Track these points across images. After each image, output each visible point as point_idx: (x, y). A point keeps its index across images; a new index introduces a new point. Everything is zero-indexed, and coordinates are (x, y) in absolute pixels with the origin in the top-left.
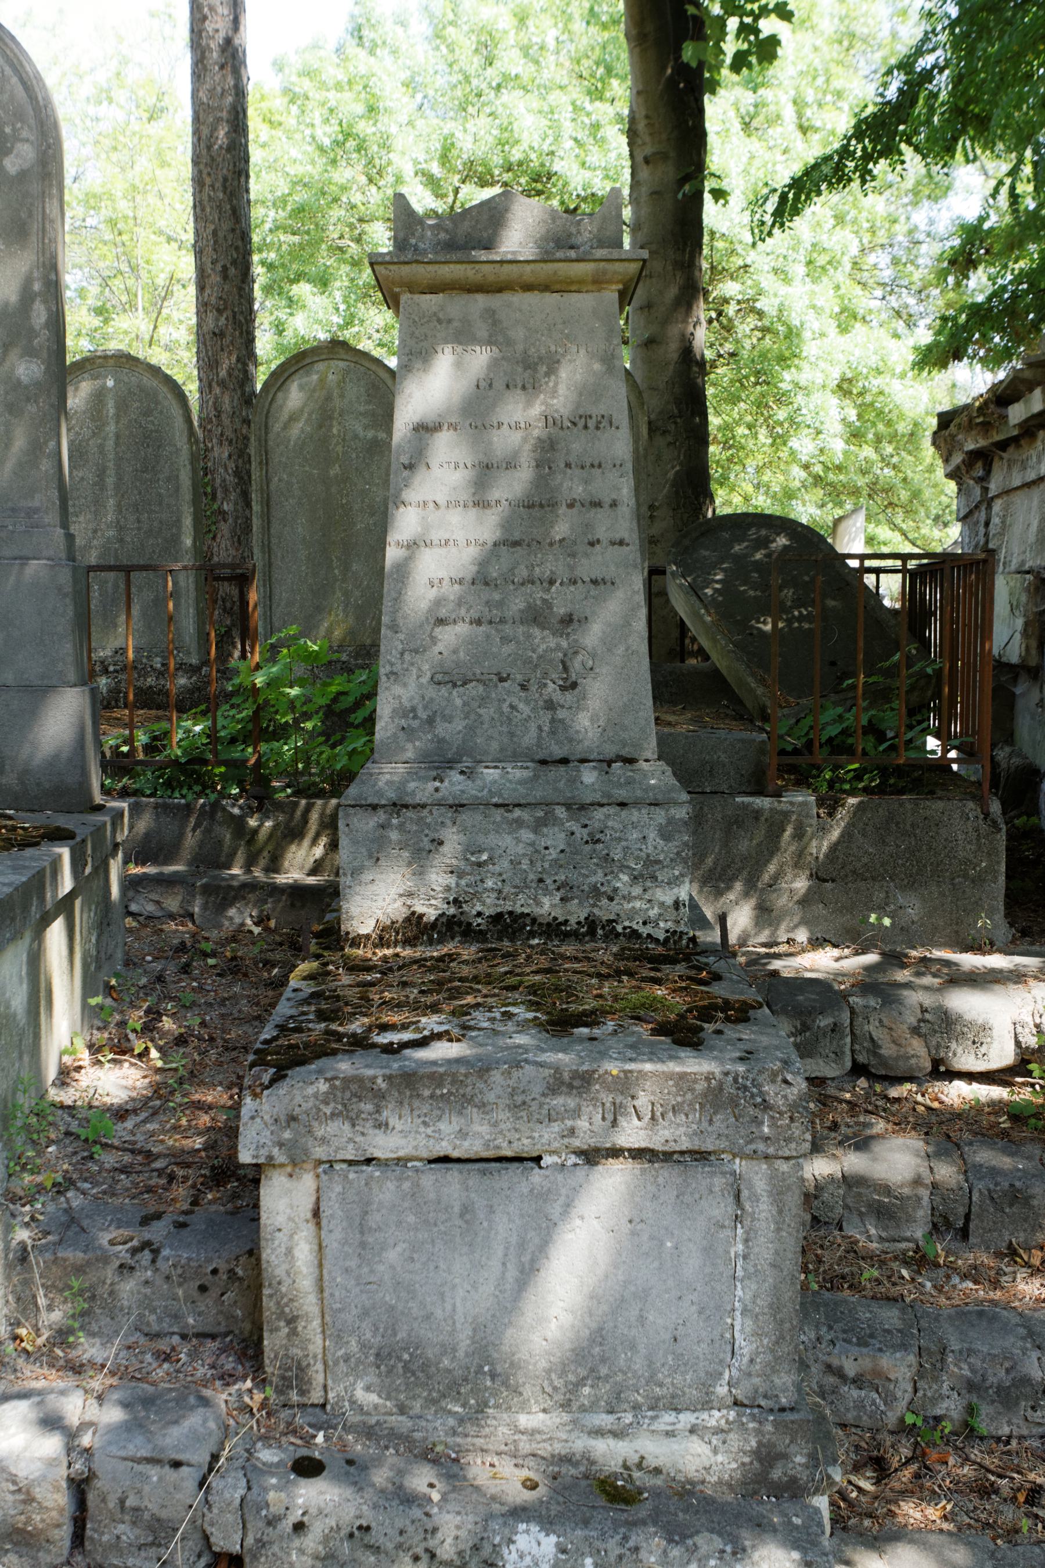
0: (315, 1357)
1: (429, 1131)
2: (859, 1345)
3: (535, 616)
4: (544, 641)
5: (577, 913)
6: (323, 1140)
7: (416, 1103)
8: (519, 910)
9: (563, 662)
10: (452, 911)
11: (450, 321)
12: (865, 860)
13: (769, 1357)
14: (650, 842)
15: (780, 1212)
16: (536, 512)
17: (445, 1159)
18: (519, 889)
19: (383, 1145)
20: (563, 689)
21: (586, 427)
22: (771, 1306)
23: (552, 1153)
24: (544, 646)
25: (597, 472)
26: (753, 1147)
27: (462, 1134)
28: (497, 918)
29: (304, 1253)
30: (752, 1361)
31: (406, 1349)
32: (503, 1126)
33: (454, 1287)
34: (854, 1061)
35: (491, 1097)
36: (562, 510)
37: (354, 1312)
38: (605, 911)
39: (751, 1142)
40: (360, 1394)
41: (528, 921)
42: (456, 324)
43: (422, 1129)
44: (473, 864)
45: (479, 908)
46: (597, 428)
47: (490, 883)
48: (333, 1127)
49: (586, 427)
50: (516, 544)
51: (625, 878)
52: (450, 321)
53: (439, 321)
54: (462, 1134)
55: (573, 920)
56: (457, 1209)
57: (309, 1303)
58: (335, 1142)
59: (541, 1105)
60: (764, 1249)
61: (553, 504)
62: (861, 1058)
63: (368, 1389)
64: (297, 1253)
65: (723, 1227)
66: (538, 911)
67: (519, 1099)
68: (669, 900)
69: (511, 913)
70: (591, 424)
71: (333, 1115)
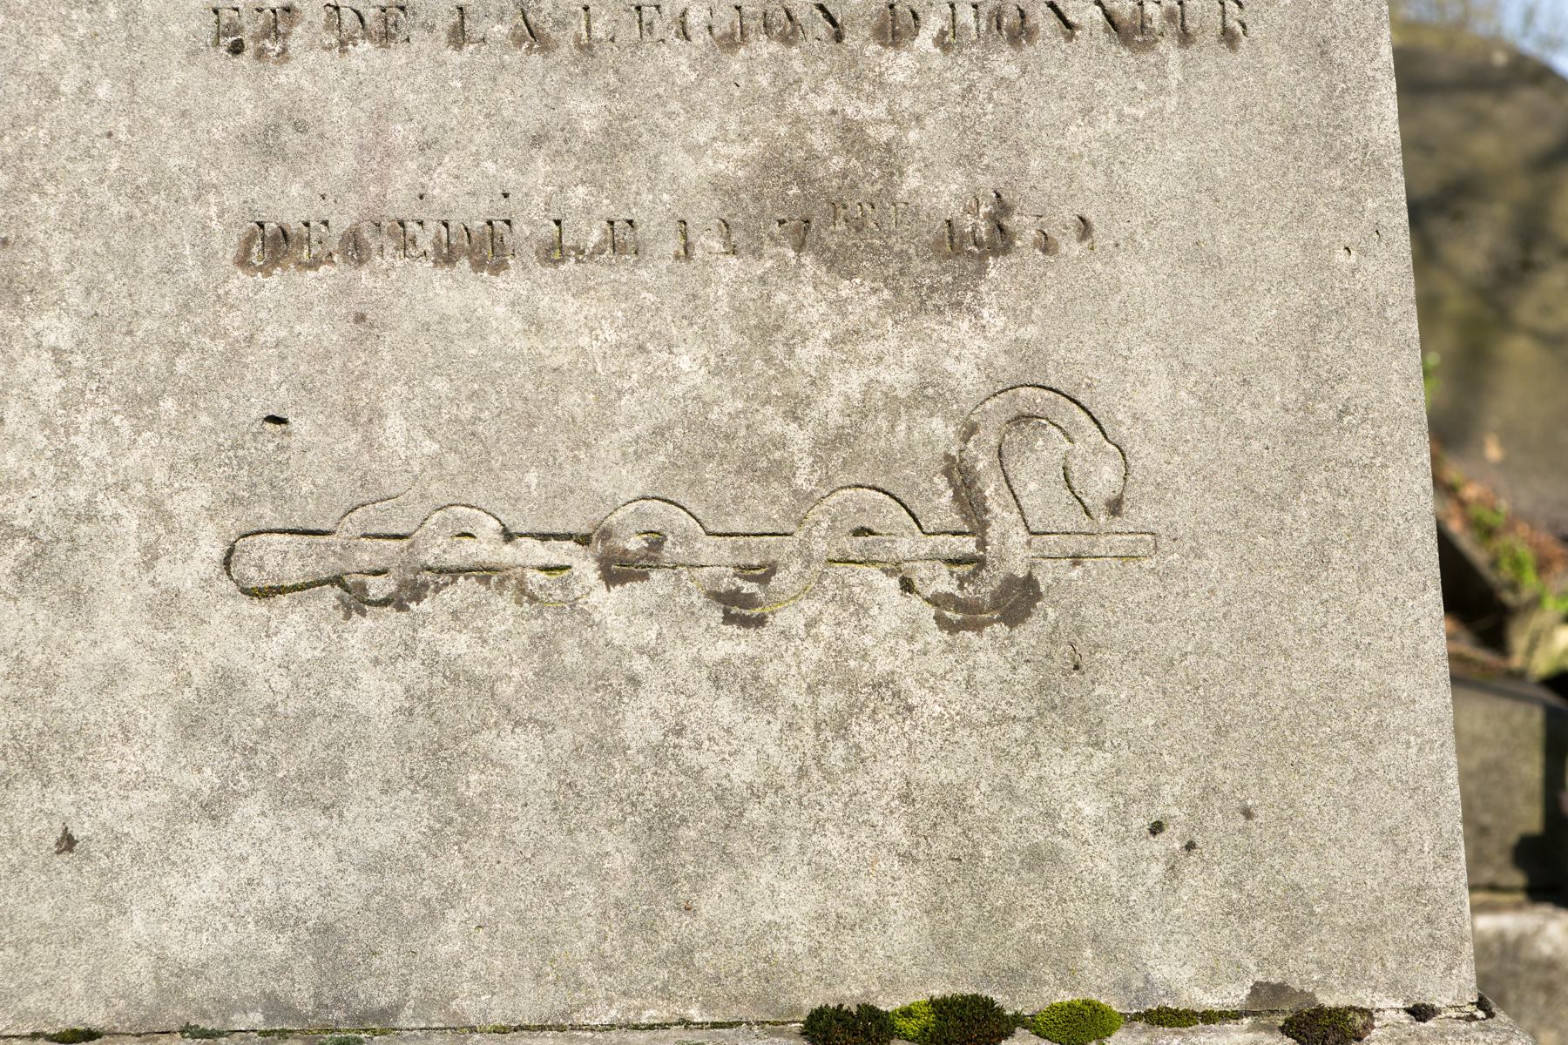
3: (814, 214)
4: (867, 355)
20: (958, 616)
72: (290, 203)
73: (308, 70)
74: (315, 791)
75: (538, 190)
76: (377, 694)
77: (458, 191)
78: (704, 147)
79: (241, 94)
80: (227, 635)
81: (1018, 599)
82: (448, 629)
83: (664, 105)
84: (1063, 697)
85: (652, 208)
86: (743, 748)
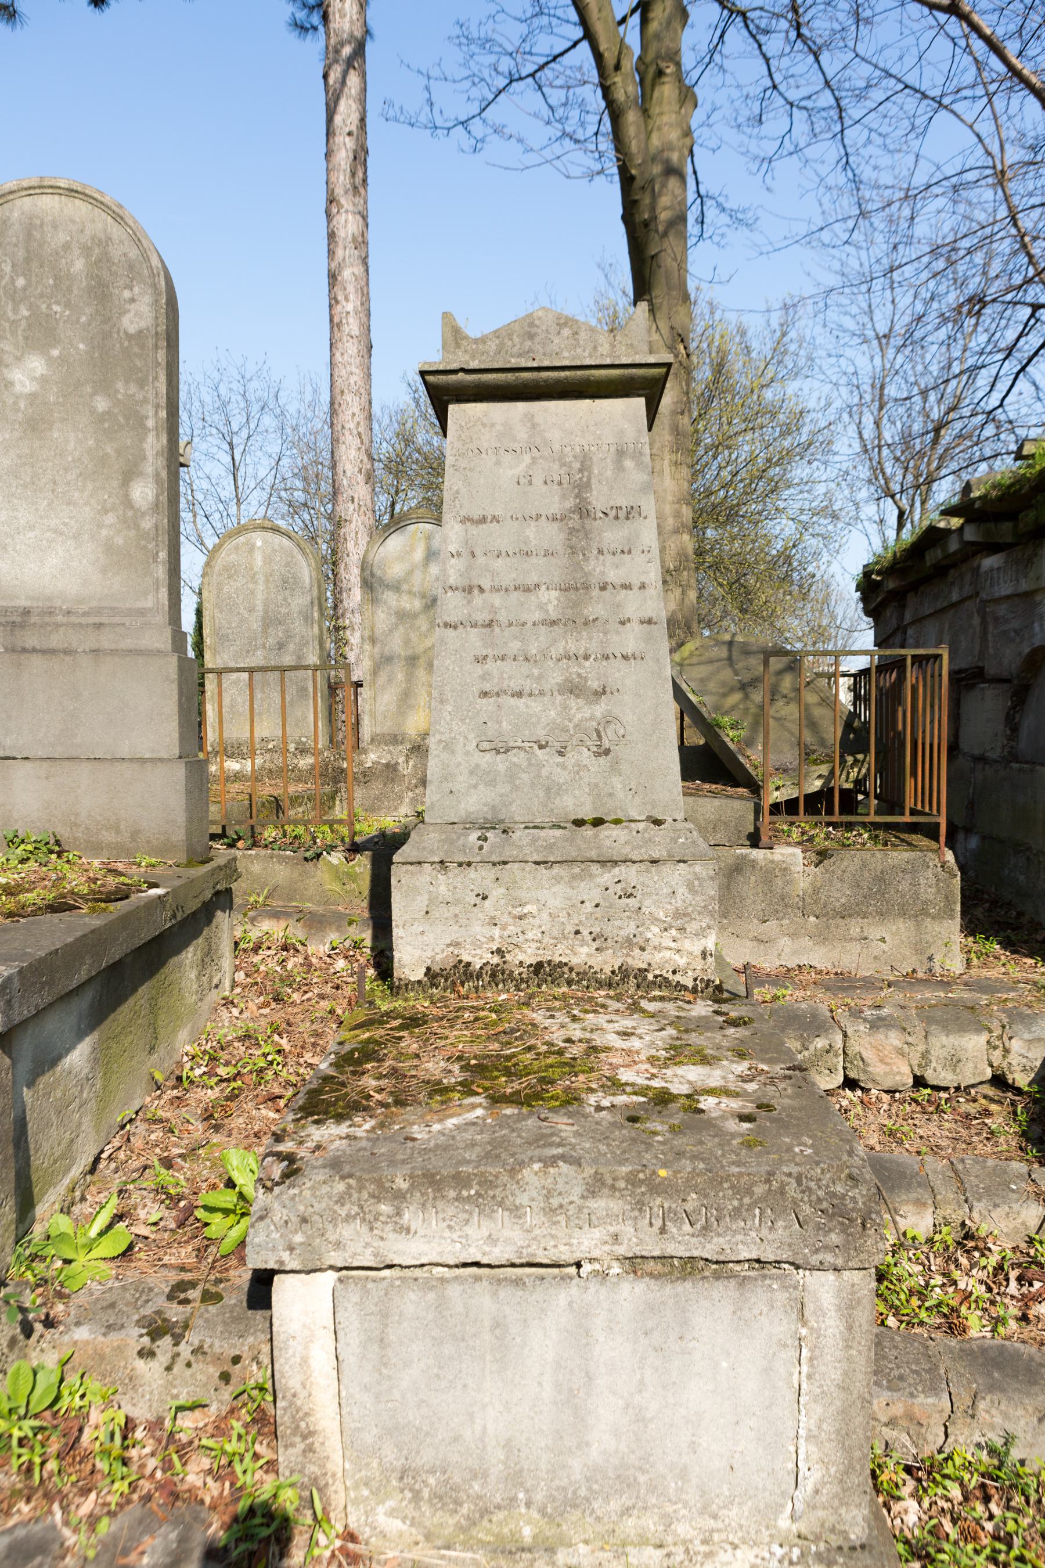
0: (334, 1475)
1: (455, 1236)
2: (890, 1389)
3: (573, 689)
4: (581, 711)
5: (606, 962)
6: (338, 1245)
7: (440, 1204)
8: (557, 959)
9: (598, 732)
10: (496, 960)
11: (493, 425)
12: (843, 900)
13: (836, 1488)
14: (679, 895)
15: (850, 1328)
16: (572, 594)
18: (557, 941)
19: (406, 1250)
20: (598, 755)
21: (617, 518)
22: (838, 1432)
23: (591, 1260)
24: (579, 716)
25: (626, 557)
26: (820, 1256)
27: (491, 1239)
28: (539, 966)
29: (321, 1360)
30: (817, 1492)
31: (432, 1471)
32: (537, 1232)
33: (484, 1407)
34: (846, 1076)
35: (522, 1199)
36: (595, 593)
37: (375, 1431)
38: (638, 960)
39: (817, 1251)
40: (382, 1519)
41: (566, 969)
42: (498, 427)
43: (447, 1233)
44: (515, 917)
45: (521, 957)
46: (628, 518)
47: (530, 935)
48: (346, 1231)
49: (617, 518)
50: (553, 623)
51: (656, 930)
52: (493, 425)
53: (484, 425)
54: (491, 1239)
55: (607, 970)
56: (487, 1323)
57: (325, 1417)
58: (352, 1247)
59: (580, 1209)
60: (832, 1372)
61: (587, 588)
62: (852, 1075)
63: (391, 1513)
64: (314, 1364)
65: (785, 1346)
66: (575, 961)
67: (555, 1202)
68: (697, 950)
69: (549, 962)
70: (622, 514)
71: (349, 1218)
72: (487, 687)
73: (490, 666)
74: (492, 783)
75: (528, 685)
76: (502, 768)
77: (514, 685)
78: (555, 678)
79: (479, 670)
81: (607, 752)
82: (514, 757)
85: (547, 687)
86: (561, 777)
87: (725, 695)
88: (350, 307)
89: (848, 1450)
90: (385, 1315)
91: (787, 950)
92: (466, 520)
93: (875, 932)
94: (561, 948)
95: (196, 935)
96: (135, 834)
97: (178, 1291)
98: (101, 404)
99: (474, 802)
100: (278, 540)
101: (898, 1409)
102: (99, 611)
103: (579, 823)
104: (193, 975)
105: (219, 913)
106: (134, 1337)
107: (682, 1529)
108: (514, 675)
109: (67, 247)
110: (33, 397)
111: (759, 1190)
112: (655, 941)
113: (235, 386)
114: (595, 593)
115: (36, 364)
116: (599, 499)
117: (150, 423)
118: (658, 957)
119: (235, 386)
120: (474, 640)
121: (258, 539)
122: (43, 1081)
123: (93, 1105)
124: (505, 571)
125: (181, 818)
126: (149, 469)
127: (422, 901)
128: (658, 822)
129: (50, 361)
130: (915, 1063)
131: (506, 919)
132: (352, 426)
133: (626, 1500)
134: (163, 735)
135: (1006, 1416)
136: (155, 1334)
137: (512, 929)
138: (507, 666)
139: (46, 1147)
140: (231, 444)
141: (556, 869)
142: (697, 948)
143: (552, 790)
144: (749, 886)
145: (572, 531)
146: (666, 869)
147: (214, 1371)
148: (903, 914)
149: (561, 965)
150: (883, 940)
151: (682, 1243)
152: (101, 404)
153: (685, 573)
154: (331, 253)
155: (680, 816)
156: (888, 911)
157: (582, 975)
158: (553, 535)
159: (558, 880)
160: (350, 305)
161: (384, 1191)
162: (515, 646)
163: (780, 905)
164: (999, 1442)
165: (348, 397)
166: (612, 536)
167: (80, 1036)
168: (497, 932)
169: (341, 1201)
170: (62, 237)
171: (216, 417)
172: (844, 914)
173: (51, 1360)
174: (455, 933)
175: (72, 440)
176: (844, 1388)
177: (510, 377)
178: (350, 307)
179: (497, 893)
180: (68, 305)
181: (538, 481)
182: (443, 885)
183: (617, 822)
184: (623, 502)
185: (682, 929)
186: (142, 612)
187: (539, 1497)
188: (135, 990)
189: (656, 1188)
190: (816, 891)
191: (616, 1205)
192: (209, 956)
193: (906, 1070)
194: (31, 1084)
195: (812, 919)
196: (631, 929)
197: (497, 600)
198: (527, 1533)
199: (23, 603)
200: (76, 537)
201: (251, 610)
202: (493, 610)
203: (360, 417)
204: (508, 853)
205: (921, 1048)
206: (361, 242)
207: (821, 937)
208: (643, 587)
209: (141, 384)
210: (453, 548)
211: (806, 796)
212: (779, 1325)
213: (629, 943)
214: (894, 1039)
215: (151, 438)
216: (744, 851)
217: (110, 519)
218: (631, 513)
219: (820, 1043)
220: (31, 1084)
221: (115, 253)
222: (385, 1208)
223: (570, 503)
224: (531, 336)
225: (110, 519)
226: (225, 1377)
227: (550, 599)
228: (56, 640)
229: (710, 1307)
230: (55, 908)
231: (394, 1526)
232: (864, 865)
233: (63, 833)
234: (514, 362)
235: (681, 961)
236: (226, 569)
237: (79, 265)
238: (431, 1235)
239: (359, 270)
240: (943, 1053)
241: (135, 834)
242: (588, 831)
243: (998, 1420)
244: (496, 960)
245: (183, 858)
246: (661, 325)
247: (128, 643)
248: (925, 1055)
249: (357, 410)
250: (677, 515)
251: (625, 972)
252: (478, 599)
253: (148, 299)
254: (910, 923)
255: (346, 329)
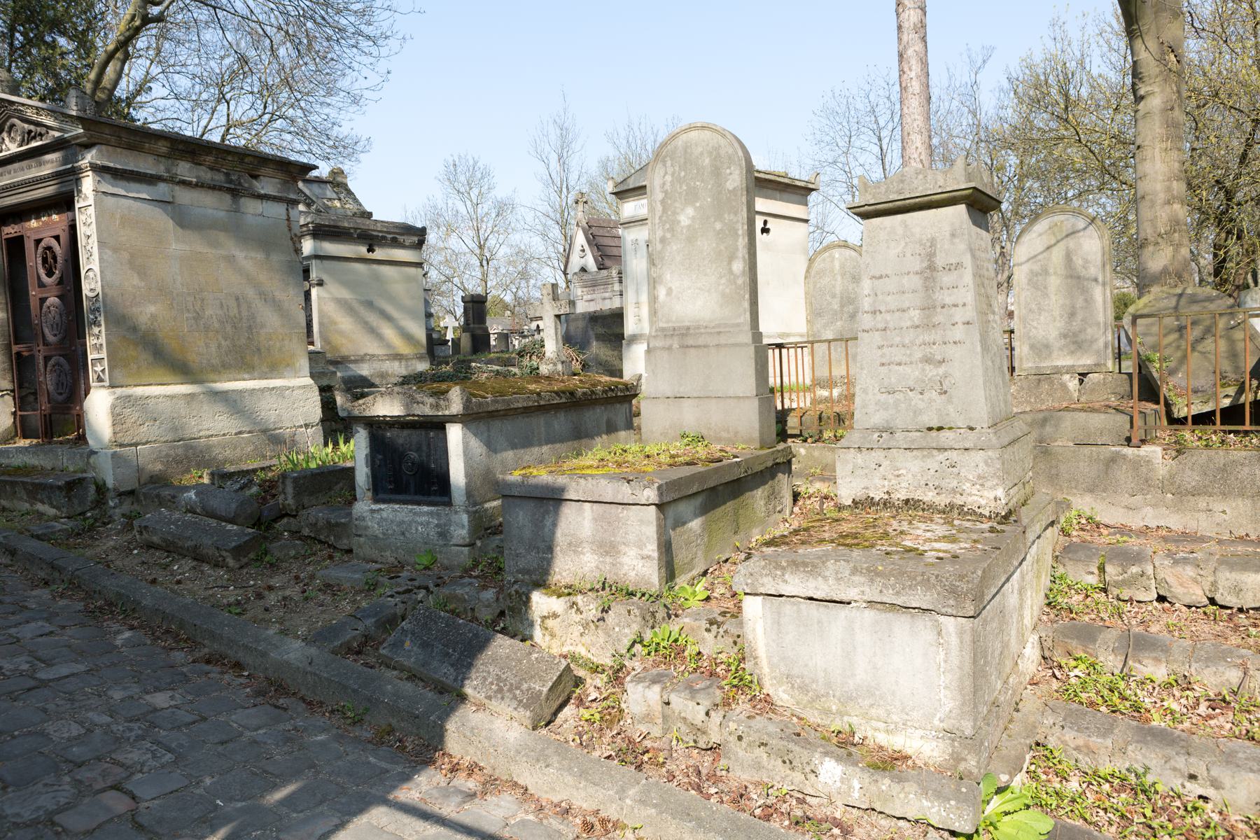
3: (928, 360)
4: (932, 372)
5: (942, 501)
6: (763, 585)
10: (886, 497)
16: (927, 312)
17: (811, 599)
18: (916, 488)
20: (940, 394)
28: (907, 501)
35: (827, 574)
36: (939, 310)
38: (959, 501)
48: (765, 580)
57: (762, 652)
60: (955, 661)
63: (784, 691)
66: (925, 499)
72: (884, 361)
73: (885, 350)
74: (886, 409)
75: (904, 359)
76: (891, 401)
77: (897, 359)
78: (918, 355)
79: (880, 352)
80: (879, 396)
81: (945, 392)
82: (897, 396)
83: (134, 814)
84: (950, 401)
85: (914, 360)
86: (921, 405)
87: (1165, 335)
88: (913, 74)
89: (964, 696)
90: (779, 613)
91: (1149, 515)
92: (873, 277)
93: (1218, 506)
94: (918, 492)
95: (764, 483)
96: (736, 433)
97: (723, 614)
98: (718, 226)
99: (878, 419)
100: (848, 252)
101: (1080, 742)
102: (719, 326)
103: (930, 429)
104: (762, 503)
105: (780, 475)
106: (705, 624)
107: (895, 718)
108: (898, 355)
109: (702, 154)
110: (689, 226)
111: (919, 578)
112: (968, 491)
113: (881, 92)
114: (939, 310)
115: (690, 211)
116: (940, 261)
117: (740, 232)
118: (970, 499)
119: (881, 92)
120: (877, 337)
121: (837, 253)
122: (678, 530)
123: (702, 547)
124: (893, 303)
125: (757, 426)
126: (740, 255)
127: (850, 467)
128: (972, 429)
129: (696, 209)
130: (1207, 588)
131: (890, 476)
132: (916, 156)
133: (871, 701)
134: (748, 385)
135: (1144, 756)
136: (711, 623)
137: (893, 482)
138: (893, 350)
139: (680, 557)
140: (880, 140)
141: (915, 452)
142: (991, 495)
143: (917, 412)
144: (1122, 474)
145: (926, 279)
146: (972, 453)
147: (731, 640)
148: (1242, 495)
149: (919, 501)
150: (1224, 512)
151: (888, 598)
152: (718, 226)
153: (1176, 235)
154: (900, 39)
155: (985, 426)
156: (1230, 493)
157: (930, 507)
158: (916, 282)
159: (916, 458)
160: (914, 70)
161: (778, 566)
162: (898, 339)
163: (1145, 482)
164: (1141, 771)
165: (913, 137)
166: (946, 279)
167: (696, 516)
168: (886, 483)
169: (763, 568)
170: (700, 149)
171: (868, 119)
172: (1195, 492)
173: (676, 629)
174: (866, 482)
175: (706, 245)
176: (960, 668)
177: (890, 205)
178: (913, 74)
179: (885, 463)
180: (702, 181)
181: (908, 255)
182: (860, 459)
183: (950, 428)
184: (954, 261)
185: (982, 485)
186: (738, 325)
187: (838, 694)
188: (724, 503)
189: (878, 574)
190: (1172, 476)
191: (863, 579)
192: (773, 496)
193: (1200, 592)
194: (674, 529)
195: (1169, 495)
196: (955, 484)
197: (888, 317)
198: (834, 708)
199: (687, 324)
200: (709, 291)
201: (834, 296)
202: (887, 322)
203: (922, 149)
204: (892, 444)
205: (1211, 579)
206: (921, 28)
207: (1177, 507)
208: (964, 305)
209: (736, 214)
210: (866, 292)
211: (1222, 410)
212: (930, 636)
213: (954, 491)
214: (1190, 571)
215: (740, 240)
216: (1118, 448)
217: (723, 281)
218: (959, 265)
219: (1135, 569)
220: (674, 529)
221: (722, 152)
222: (779, 573)
223: (925, 264)
224: (902, 181)
225: (723, 281)
226: (735, 643)
227: (915, 315)
228: (701, 341)
229: (901, 623)
230: (688, 464)
231: (785, 697)
232: (1210, 459)
233: (705, 432)
234: (892, 197)
235: (983, 502)
236: (817, 273)
237: (707, 161)
238: (794, 584)
239: (919, 47)
240: (1228, 584)
241: (736, 433)
242: (934, 433)
243: (1140, 757)
244: (886, 497)
245: (758, 446)
246: (1149, 44)
247: (732, 341)
248: (1214, 584)
249: (919, 145)
250: (1169, 189)
251: (951, 506)
252: (879, 317)
253: (737, 172)
254: (1248, 502)
255: (910, 90)
